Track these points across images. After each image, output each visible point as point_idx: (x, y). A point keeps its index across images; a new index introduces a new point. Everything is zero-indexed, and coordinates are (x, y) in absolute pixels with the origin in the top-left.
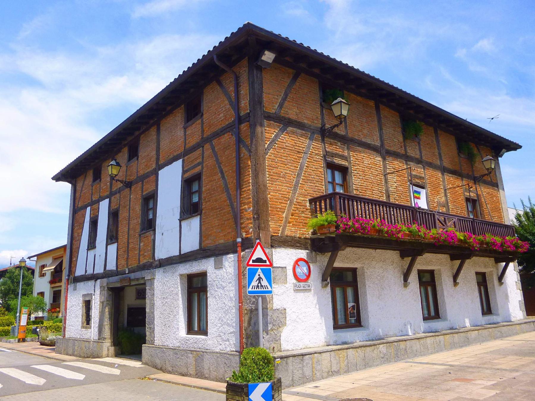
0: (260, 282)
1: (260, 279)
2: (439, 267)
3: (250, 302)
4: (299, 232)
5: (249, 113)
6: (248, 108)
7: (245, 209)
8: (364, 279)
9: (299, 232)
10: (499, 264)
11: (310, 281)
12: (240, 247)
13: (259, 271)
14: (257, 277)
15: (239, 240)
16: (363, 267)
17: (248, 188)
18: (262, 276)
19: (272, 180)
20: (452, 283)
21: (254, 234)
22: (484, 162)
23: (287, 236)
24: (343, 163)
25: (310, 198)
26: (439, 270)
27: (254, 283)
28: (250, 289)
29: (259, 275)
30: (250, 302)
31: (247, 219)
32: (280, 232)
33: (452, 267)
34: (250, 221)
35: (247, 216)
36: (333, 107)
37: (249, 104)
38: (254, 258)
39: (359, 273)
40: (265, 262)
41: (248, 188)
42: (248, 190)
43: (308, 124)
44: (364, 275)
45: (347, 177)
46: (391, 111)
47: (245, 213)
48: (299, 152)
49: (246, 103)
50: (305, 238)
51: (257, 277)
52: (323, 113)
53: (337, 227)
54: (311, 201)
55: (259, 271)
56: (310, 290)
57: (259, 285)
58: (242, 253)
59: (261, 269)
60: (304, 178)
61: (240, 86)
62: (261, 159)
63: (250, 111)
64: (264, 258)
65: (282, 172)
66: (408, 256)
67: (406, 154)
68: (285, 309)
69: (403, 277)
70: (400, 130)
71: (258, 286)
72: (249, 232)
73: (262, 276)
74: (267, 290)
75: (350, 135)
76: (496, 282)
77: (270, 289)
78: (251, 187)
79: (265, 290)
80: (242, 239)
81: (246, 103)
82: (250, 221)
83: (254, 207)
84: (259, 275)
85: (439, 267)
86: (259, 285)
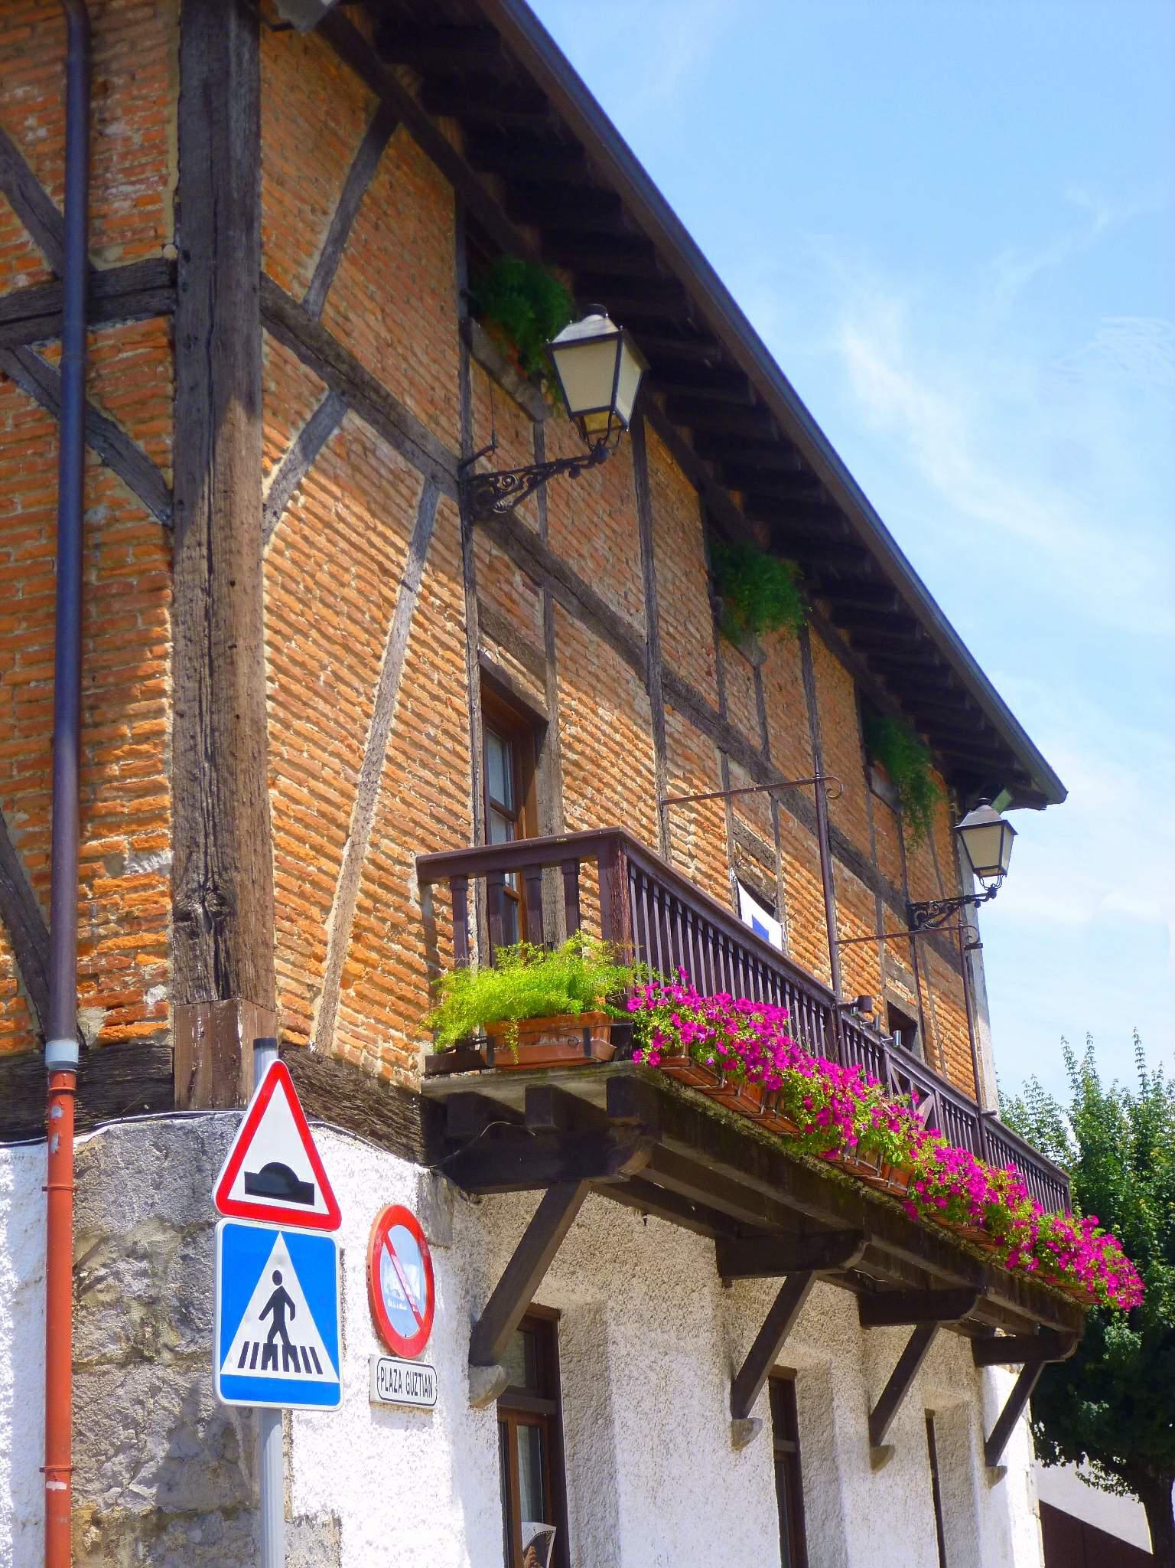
0: (279, 1326)
1: (279, 1301)
2: (826, 1356)
3: (135, 1467)
4: (382, 1045)
5: (173, 266)
6: (169, 230)
7: (113, 861)
8: (603, 1376)
9: (382, 1045)
10: (984, 1370)
11: (429, 1356)
12: (68, 1101)
13: (280, 1248)
14: (264, 1291)
15: (65, 1051)
16: (598, 1309)
17: (145, 725)
18: (292, 1285)
19: (286, 698)
20: (865, 1447)
21: (185, 1018)
22: (965, 833)
23: (339, 1060)
24: (532, 691)
25: (423, 852)
26: (824, 1374)
27: (253, 1329)
28: (231, 1368)
29: (277, 1277)
30: (135, 1467)
31: (129, 920)
32: (314, 1027)
33: (866, 1358)
34: (149, 938)
35: (134, 903)
36: (559, 357)
37: (178, 210)
38: (253, 1163)
39: (569, 1341)
40: (304, 1193)
41: (145, 725)
42: (145, 738)
43: (415, 416)
44: (603, 1357)
45: (539, 776)
46: (677, 469)
47: (105, 881)
48: (386, 572)
49: (155, 199)
50: (404, 1092)
51: (264, 1291)
52: (468, 384)
53: (625, 1036)
54: (429, 870)
55: (280, 1248)
56: (428, 1410)
57: (278, 1340)
58: (77, 1140)
59: (286, 1235)
60: (401, 728)
61: (106, 89)
62: (247, 562)
63: (186, 256)
64: (305, 1173)
65: (324, 667)
66: (772, 1271)
67: (722, 716)
68: (338, 1522)
69: (728, 1386)
70: (702, 578)
71: (270, 1350)
72: (135, 1002)
73: (292, 1285)
74: (314, 1377)
75: (555, 544)
76: (978, 1460)
77: (328, 1376)
78: (167, 722)
79: (303, 1376)
80: (83, 1049)
81: (155, 199)
82: (149, 938)
83: (186, 846)
84: (277, 1277)
85: (826, 1356)
86: (278, 1340)
